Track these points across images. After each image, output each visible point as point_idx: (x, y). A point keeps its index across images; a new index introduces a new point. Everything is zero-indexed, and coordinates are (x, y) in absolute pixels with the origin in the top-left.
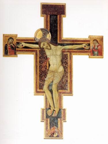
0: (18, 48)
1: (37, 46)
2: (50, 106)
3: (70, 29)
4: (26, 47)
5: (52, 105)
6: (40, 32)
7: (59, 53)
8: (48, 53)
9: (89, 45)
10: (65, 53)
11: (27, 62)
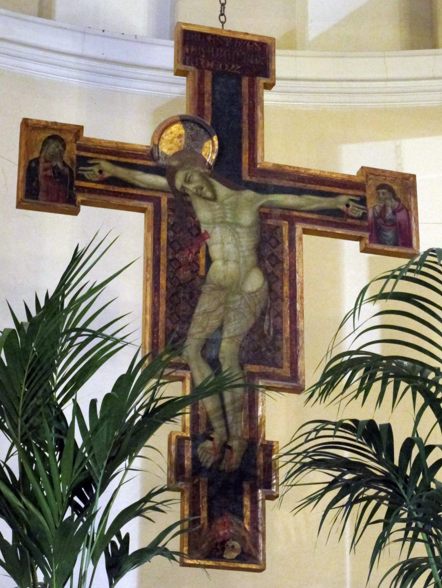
0: (82, 178)
1: (161, 181)
3: (292, 130)
4: (114, 180)
6: (177, 129)
7: (247, 218)
8: (204, 213)
9: (363, 201)
10: (270, 222)
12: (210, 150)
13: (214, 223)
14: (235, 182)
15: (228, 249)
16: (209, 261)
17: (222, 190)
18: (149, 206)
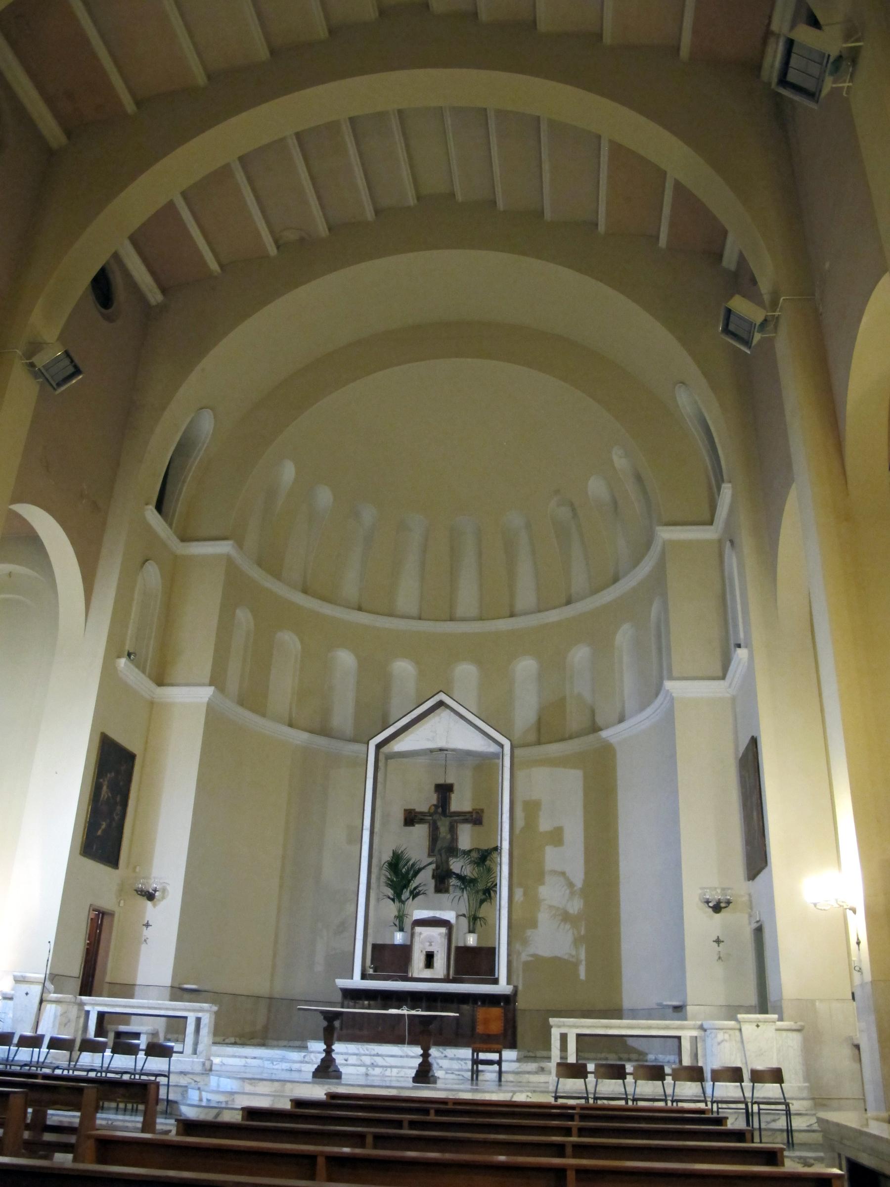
8: (439, 823)
11: (420, 831)
15: (443, 830)
17: (443, 818)
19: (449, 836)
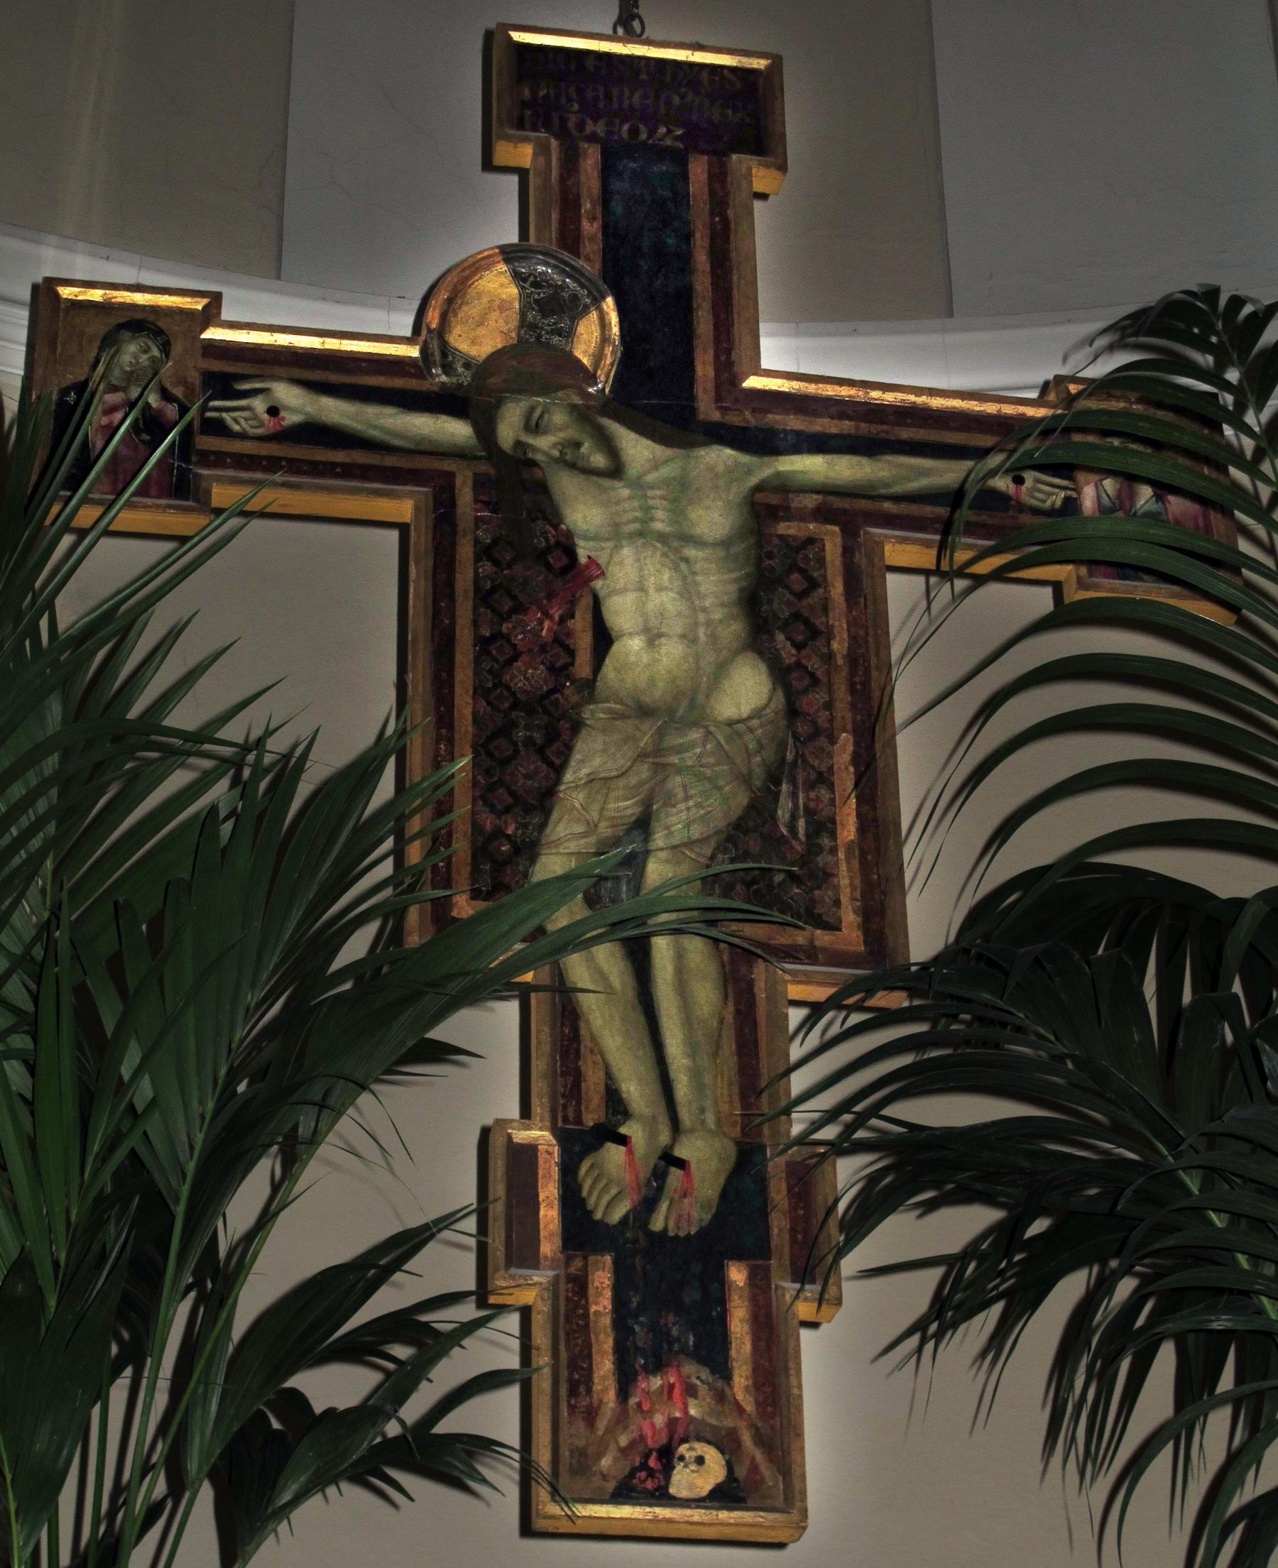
1: (457, 430)
2: (616, 1103)
5: (636, 1089)
7: (714, 518)
8: (584, 512)
12: (596, 335)
13: (616, 534)
14: (677, 424)
16: (604, 639)
17: (638, 449)
18: (403, 507)
19: (747, 690)
